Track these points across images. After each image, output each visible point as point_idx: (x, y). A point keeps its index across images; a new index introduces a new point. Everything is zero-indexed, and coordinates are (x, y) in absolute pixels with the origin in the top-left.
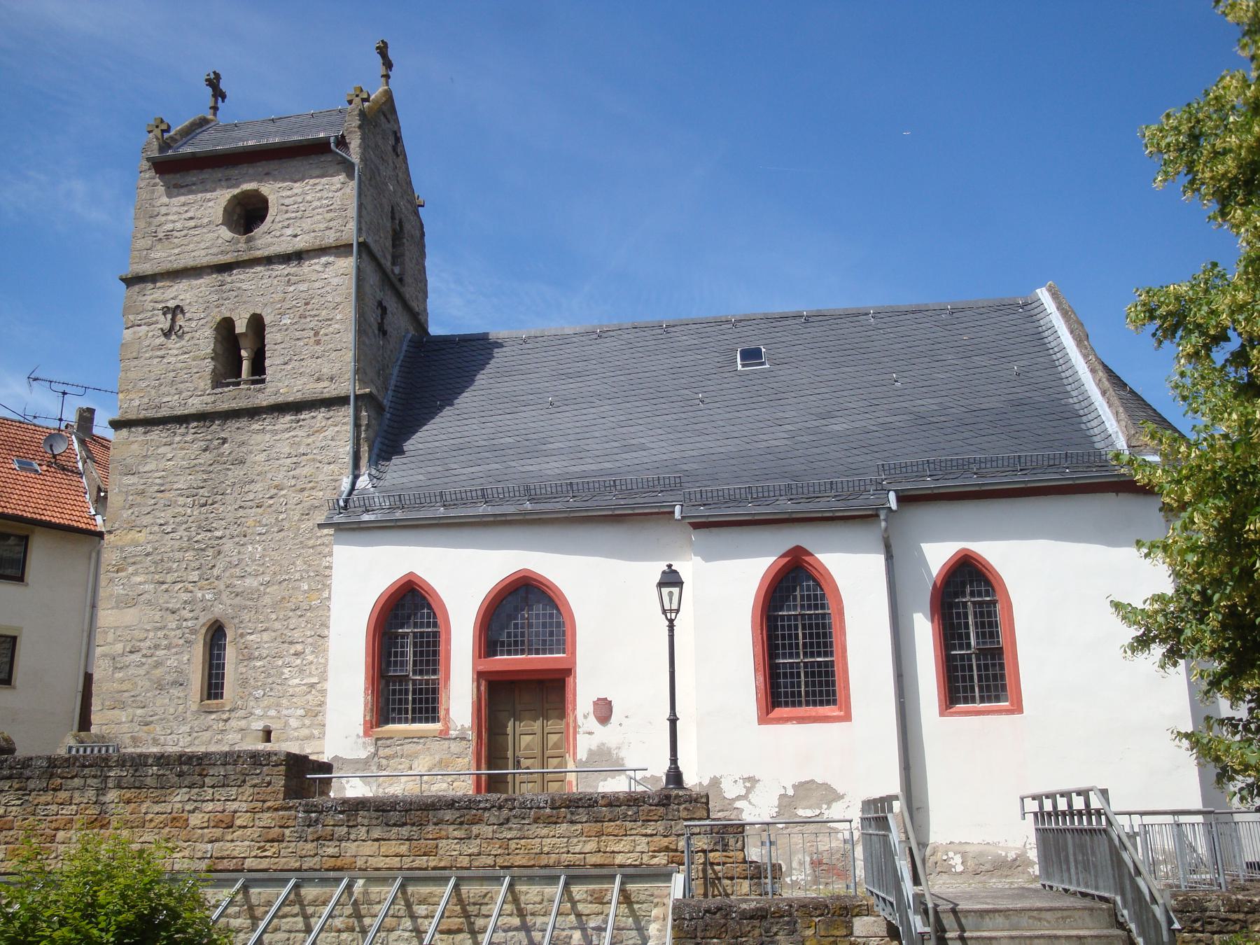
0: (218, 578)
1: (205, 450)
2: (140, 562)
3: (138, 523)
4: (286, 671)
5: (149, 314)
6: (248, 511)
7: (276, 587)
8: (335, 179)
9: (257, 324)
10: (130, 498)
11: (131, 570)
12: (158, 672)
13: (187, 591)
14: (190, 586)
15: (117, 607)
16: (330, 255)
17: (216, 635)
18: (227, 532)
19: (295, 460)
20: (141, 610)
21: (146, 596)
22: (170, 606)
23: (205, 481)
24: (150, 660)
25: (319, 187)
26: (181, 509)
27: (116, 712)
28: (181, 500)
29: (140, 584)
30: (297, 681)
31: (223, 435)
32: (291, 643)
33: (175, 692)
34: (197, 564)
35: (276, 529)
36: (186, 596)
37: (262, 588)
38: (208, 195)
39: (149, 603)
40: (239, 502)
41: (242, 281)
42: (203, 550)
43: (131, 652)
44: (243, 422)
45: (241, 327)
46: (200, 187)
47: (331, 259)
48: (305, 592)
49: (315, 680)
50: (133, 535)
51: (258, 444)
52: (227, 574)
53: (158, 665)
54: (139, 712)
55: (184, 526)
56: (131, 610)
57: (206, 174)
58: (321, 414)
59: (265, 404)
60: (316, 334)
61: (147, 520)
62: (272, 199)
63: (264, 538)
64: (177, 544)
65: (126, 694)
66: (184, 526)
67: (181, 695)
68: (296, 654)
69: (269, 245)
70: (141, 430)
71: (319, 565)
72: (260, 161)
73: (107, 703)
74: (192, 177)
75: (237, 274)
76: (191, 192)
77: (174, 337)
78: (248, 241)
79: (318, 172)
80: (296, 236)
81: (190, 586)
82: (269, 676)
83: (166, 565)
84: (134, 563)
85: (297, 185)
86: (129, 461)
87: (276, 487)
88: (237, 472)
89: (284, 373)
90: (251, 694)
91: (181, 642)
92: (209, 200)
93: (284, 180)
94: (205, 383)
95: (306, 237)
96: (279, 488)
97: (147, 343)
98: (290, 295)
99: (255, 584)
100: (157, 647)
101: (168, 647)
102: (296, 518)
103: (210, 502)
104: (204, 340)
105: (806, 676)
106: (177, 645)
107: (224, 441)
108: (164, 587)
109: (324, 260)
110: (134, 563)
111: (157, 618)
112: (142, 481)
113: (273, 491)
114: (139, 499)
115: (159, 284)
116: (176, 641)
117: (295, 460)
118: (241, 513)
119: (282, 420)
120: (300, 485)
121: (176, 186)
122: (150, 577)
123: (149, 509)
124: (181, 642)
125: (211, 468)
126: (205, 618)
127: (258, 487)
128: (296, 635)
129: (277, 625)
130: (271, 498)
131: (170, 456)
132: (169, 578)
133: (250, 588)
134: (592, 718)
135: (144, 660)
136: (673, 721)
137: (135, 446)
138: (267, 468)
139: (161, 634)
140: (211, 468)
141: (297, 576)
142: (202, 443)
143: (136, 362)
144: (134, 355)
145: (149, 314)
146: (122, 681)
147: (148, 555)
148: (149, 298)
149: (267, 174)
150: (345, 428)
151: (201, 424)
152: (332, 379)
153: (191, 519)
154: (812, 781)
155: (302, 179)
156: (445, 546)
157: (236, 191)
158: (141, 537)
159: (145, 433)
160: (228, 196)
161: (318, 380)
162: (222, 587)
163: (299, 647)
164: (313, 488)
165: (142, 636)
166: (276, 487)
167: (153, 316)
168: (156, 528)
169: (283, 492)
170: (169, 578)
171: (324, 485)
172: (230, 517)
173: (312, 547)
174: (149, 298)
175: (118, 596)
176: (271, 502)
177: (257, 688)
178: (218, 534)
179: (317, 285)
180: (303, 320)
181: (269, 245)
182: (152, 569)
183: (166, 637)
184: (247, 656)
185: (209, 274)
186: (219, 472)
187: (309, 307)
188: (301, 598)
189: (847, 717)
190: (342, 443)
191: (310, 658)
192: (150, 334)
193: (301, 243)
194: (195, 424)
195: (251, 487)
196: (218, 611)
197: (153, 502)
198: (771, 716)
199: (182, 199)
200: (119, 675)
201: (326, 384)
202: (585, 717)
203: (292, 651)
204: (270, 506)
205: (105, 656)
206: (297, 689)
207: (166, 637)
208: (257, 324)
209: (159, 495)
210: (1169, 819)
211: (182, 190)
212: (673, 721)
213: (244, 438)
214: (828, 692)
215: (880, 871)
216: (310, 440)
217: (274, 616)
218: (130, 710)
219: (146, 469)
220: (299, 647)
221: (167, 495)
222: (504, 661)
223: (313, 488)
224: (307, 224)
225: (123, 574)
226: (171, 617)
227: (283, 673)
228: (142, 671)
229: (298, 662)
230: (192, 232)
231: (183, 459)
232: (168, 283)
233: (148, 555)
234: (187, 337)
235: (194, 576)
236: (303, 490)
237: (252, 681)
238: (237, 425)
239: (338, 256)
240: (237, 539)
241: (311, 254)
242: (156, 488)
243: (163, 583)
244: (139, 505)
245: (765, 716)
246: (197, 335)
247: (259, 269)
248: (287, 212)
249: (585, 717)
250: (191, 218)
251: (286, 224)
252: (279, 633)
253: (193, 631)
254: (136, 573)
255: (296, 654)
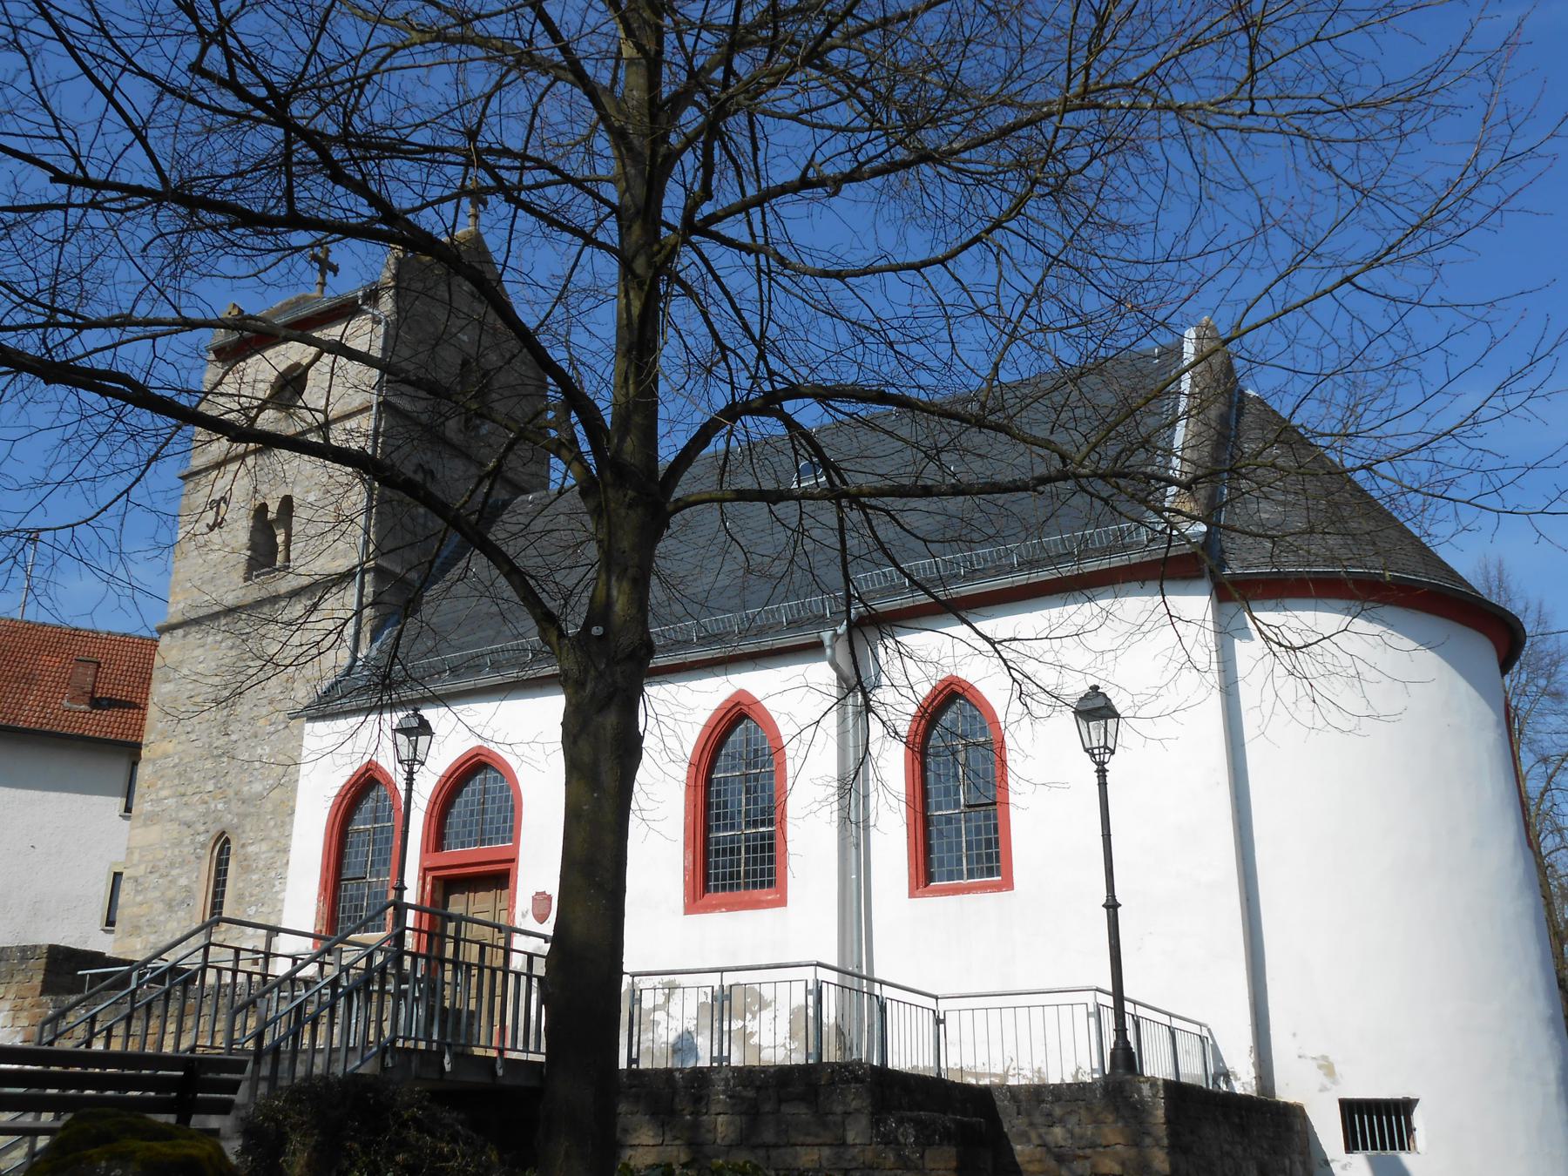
9: (287, 504)
14: (206, 797)
17: (223, 845)
36: (202, 808)
81: (206, 797)
94: (238, 575)
104: (239, 530)
105: (747, 852)
126: (214, 830)
134: (530, 916)
136: (1112, 906)
146: (141, 904)
154: (102, 954)
168: (183, 737)
184: (246, 869)
189: (782, 902)
196: (229, 819)
198: (699, 902)
200: (139, 898)
202: (524, 916)
208: (287, 504)
210: (1165, 1019)
212: (1112, 906)
214: (989, 856)
222: (442, 859)
235: (210, 787)
245: (912, 895)
249: (524, 916)
253: (203, 846)
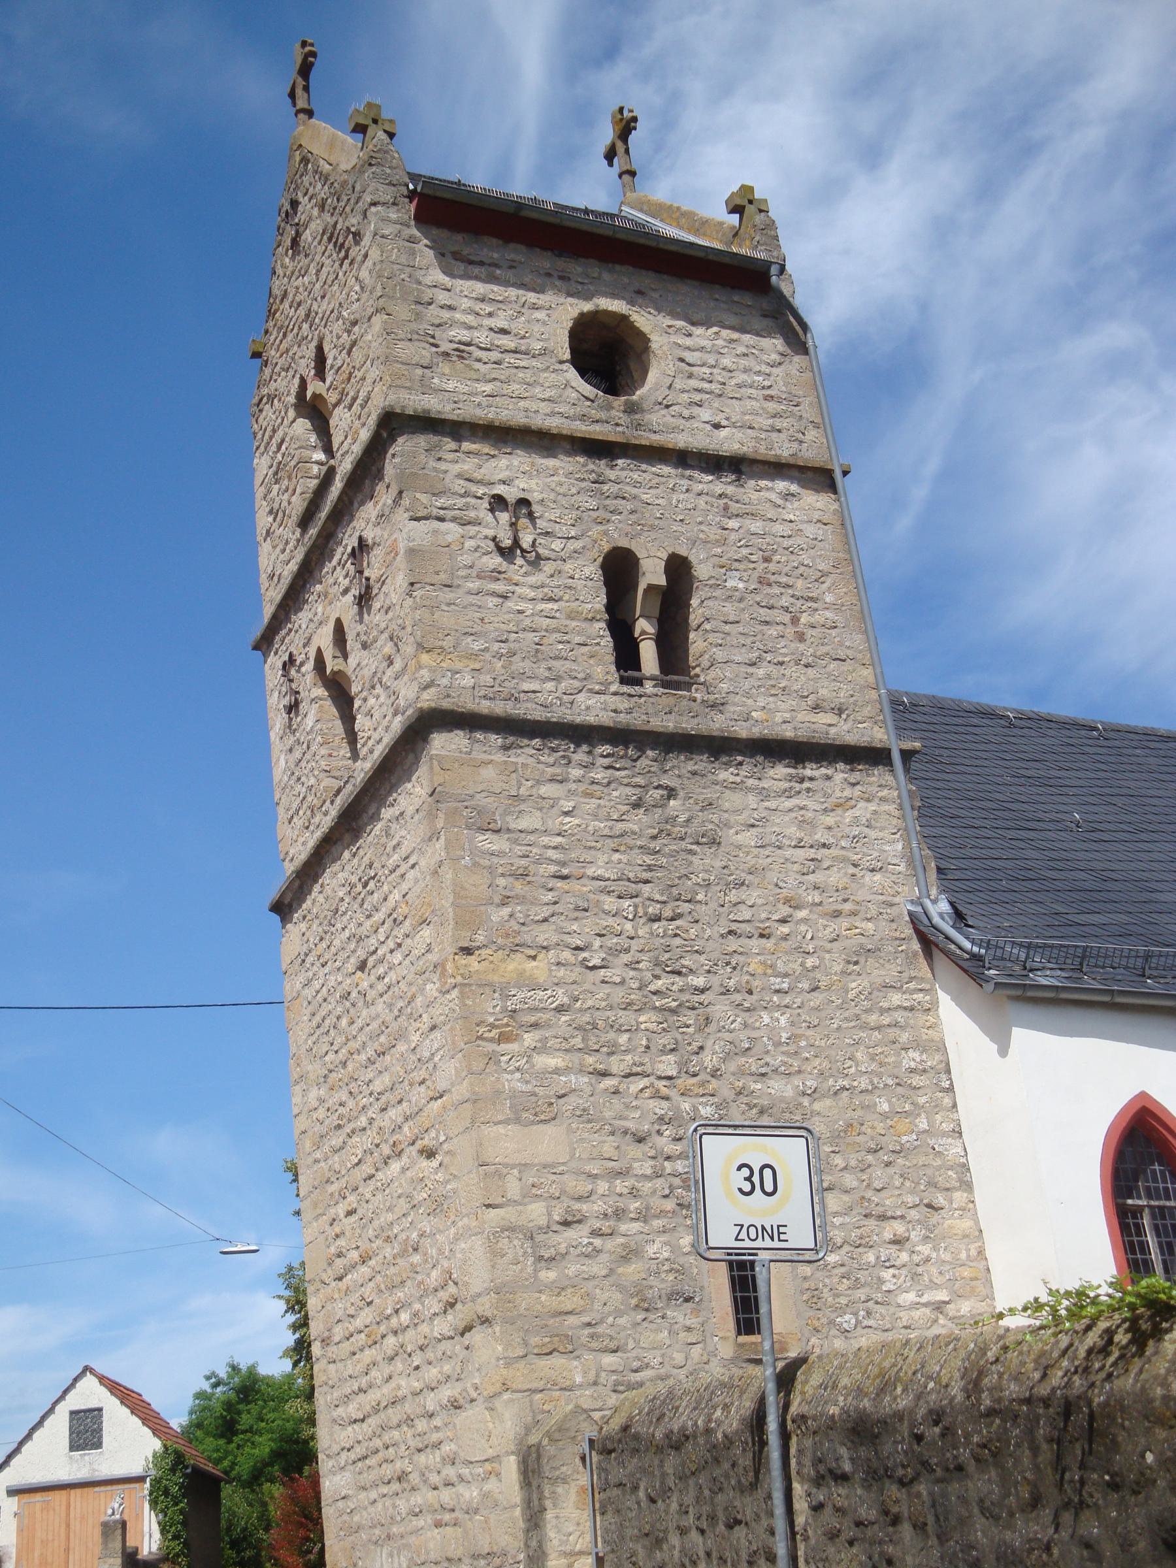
0: (715, 1073)
1: (636, 805)
2: (548, 1025)
3: (528, 939)
4: (887, 1274)
5: (460, 502)
6: (744, 941)
7: (828, 1102)
8: (766, 343)
10: (502, 882)
11: (529, 1039)
12: (632, 1271)
13: (658, 1096)
15: (517, 1120)
16: (792, 479)
18: (715, 981)
19: (812, 853)
20: (570, 1130)
21: (572, 1100)
22: (631, 1125)
23: (650, 868)
24: (610, 1244)
25: (741, 349)
26: (610, 921)
27: (557, 1361)
28: (610, 903)
29: (557, 1071)
30: (911, 1297)
31: (665, 781)
32: (883, 1218)
33: (680, 1315)
34: (665, 1040)
35: (805, 985)
37: (806, 1101)
38: (532, 297)
39: (583, 1114)
40: (723, 922)
41: (637, 484)
42: (673, 1011)
43: (566, 1224)
44: (700, 762)
45: (653, 573)
46: (510, 274)
47: (794, 488)
48: (885, 1116)
49: (942, 1296)
50: (516, 964)
51: (737, 812)
52: (732, 1066)
53: (629, 1254)
54: (608, 1360)
55: (626, 958)
56: (549, 1129)
57: (516, 253)
58: (840, 774)
59: (744, 734)
60: (795, 621)
61: (546, 934)
62: (657, 342)
63: (787, 1000)
64: (619, 995)
65: (572, 1320)
66: (626, 958)
67: (692, 1322)
68: (898, 1242)
69: (675, 429)
70: (495, 739)
71: (897, 1065)
72: (621, 262)
73: (535, 1340)
74: (490, 249)
75: (623, 470)
76: (491, 279)
77: (519, 561)
78: (632, 409)
79: (732, 320)
80: (717, 426)
82: (857, 1285)
83: (605, 1037)
84: (535, 1025)
85: (699, 331)
86: (481, 800)
87: (787, 901)
88: (706, 862)
89: (752, 681)
90: (832, 1322)
91: (669, 1205)
92: (535, 307)
93: (674, 315)
95: (739, 435)
96: (795, 904)
97: (466, 559)
98: (733, 536)
99: (789, 1092)
100: (619, 1214)
101: (643, 1216)
102: (837, 968)
103: (668, 913)
106: (662, 1213)
107: (671, 793)
108: (609, 1082)
109: (781, 485)
110: (535, 1025)
111: (608, 1149)
112: (519, 850)
113: (785, 910)
114: (519, 887)
115: (467, 446)
116: (657, 1203)
117: (812, 853)
118: (733, 944)
119: (771, 772)
120: (831, 904)
121: (457, 256)
122: (576, 1057)
123: (545, 912)
124: (669, 1205)
125: (656, 845)
127: (753, 896)
128: (888, 1201)
129: (850, 1180)
130: (783, 921)
131: (568, 805)
132: (617, 1065)
133: (782, 1099)
135: (597, 1242)
137: (488, 773)
138: (763, 862)
139: (620, 1186)
140: (656, 845)
141: (864, 1083)
142: (629, 791)
143: (449, 595)
144: (443, 577)
145: (460, 502)
146: (560, 1290)
147: (560, 1009)
148: (456, 468)
149: (639, 292)
150: (886, 807)
151: (620, 750)
152: (840, 712)
153: (635, 945)
155: (707, 324)
156: (1170, 1113)
157: (587, 307)
158: (538, 969)
159: (506, 748)
160: (575, 313)
161: (816, 708)
162: (727, 1093)
163: (899, 1228)
164: (854, 914)
165: (584, 1187)
166: (787, 901)
167: (466, 507)
168: (567, 955)
169: (802, 914)
170: (617, 1065)
171: (873, 912)
172: (714, 948)
173: (878, 1028)
174: (456, 468)
175: (514, 1095)
176: (785, 929)
177: (841, 1310)
178: (699, 981)
179: (779, 528)
180: (767, 590)
181: (675, 429)
182: (577, 1042)
183: (634, 1193)
185: (569, 454)
186: (673, 854)
187: (772, 567)
188: (880, 1127)
190: (885, 834)
191: (925, 1249)
192: (470, 544)
193: (729, 442)
194: (607, 749)
195: (743, 894)
197: (550, 896)
199: (480, 288)
201: (830, 718)
203: (888, 1235)
204: (785, 938)
205: (511, 1229)
206: (916, 1314)
207: (634, 1193)
208: (679, 569)
209: (560, 884)
211: (476, 270)
213: (710, 794)
215: (1017, 999)
216: (829, 820)
217: (838, 1161)
218: (588, 1356)
219: (523, 824)
220: (899, 1228)
221: (573, 885)
223: (854, 914)
224: (735, 410)
225: (514, 1047)
226: (635, 1151)
227: (881, 1281)
228: (597, 1268)
229: (904, 1257)
230: (509, 358)
231: (595, 816)
232: (486, 449)
233: (560, 1009)
234: (548, 567)
235: (668, 1065)
236: (837, 914)
237: (826, 1293)
238: (690, 766)
239: (804, 485)
240: (738, 997)
241: (755, 468)
242: (553, 869)
243: (605, 1074)
244: (522, 900)
246: (568, 567)
247: (666, 470)
248: (690, 376)
250: (504, 331)
251: (697, 397)
252: (856, 1196)
254: (541, 1048)
255: (898, 1242)
